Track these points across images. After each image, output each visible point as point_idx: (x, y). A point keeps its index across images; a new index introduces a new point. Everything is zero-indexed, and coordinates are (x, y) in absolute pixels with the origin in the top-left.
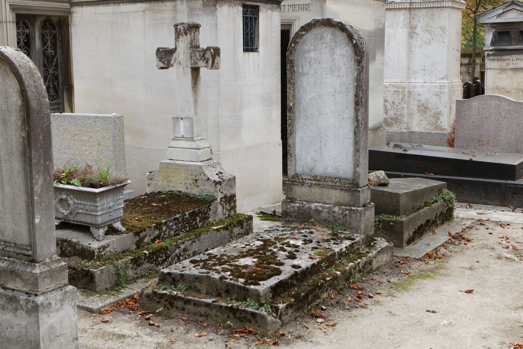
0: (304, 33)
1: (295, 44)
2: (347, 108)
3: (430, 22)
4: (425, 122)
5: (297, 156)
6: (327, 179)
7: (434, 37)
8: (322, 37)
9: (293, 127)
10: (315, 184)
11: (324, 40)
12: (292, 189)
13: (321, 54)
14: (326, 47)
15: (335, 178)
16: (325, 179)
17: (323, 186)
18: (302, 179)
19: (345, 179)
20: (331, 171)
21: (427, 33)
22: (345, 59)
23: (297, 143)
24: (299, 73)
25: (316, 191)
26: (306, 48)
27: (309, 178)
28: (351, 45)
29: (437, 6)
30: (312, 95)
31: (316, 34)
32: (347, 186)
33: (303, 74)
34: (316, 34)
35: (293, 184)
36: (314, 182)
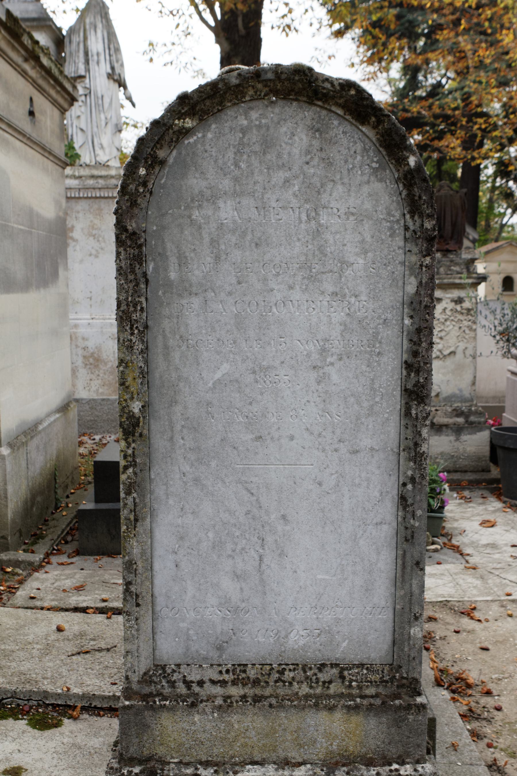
0: (189, 123)
1: (150, 168)
2: (371, 412)
3: (96, 221)
4: (96, 384)
5: (160, 601)
6: (288, 675)
7: (103, 245)
8: (267, 144)
9: (143, 496)
10: (244, 697)
11: (279, 156)
12: (146, 727)
13: (263, 208)
14: (287, 181)
15: (322, 667)
16: (282, 672)
17: (280, 704)
18: (188, 684)
19: (361, 666)
20: (301, 643)
21: (91, 238)
22: (367, 229)
23: (159, 551)
24: (168, 285)
25: (249, 726)
26: (195, 183)
27: (216, 677)
28: (390, 173)
29: (106, 195)
30: (225, 367)
31: (244, 131)
32: (372, 691)
33: (186, 289)
34: (244, 131)
35: (153, 708)
36: (235, 691)
